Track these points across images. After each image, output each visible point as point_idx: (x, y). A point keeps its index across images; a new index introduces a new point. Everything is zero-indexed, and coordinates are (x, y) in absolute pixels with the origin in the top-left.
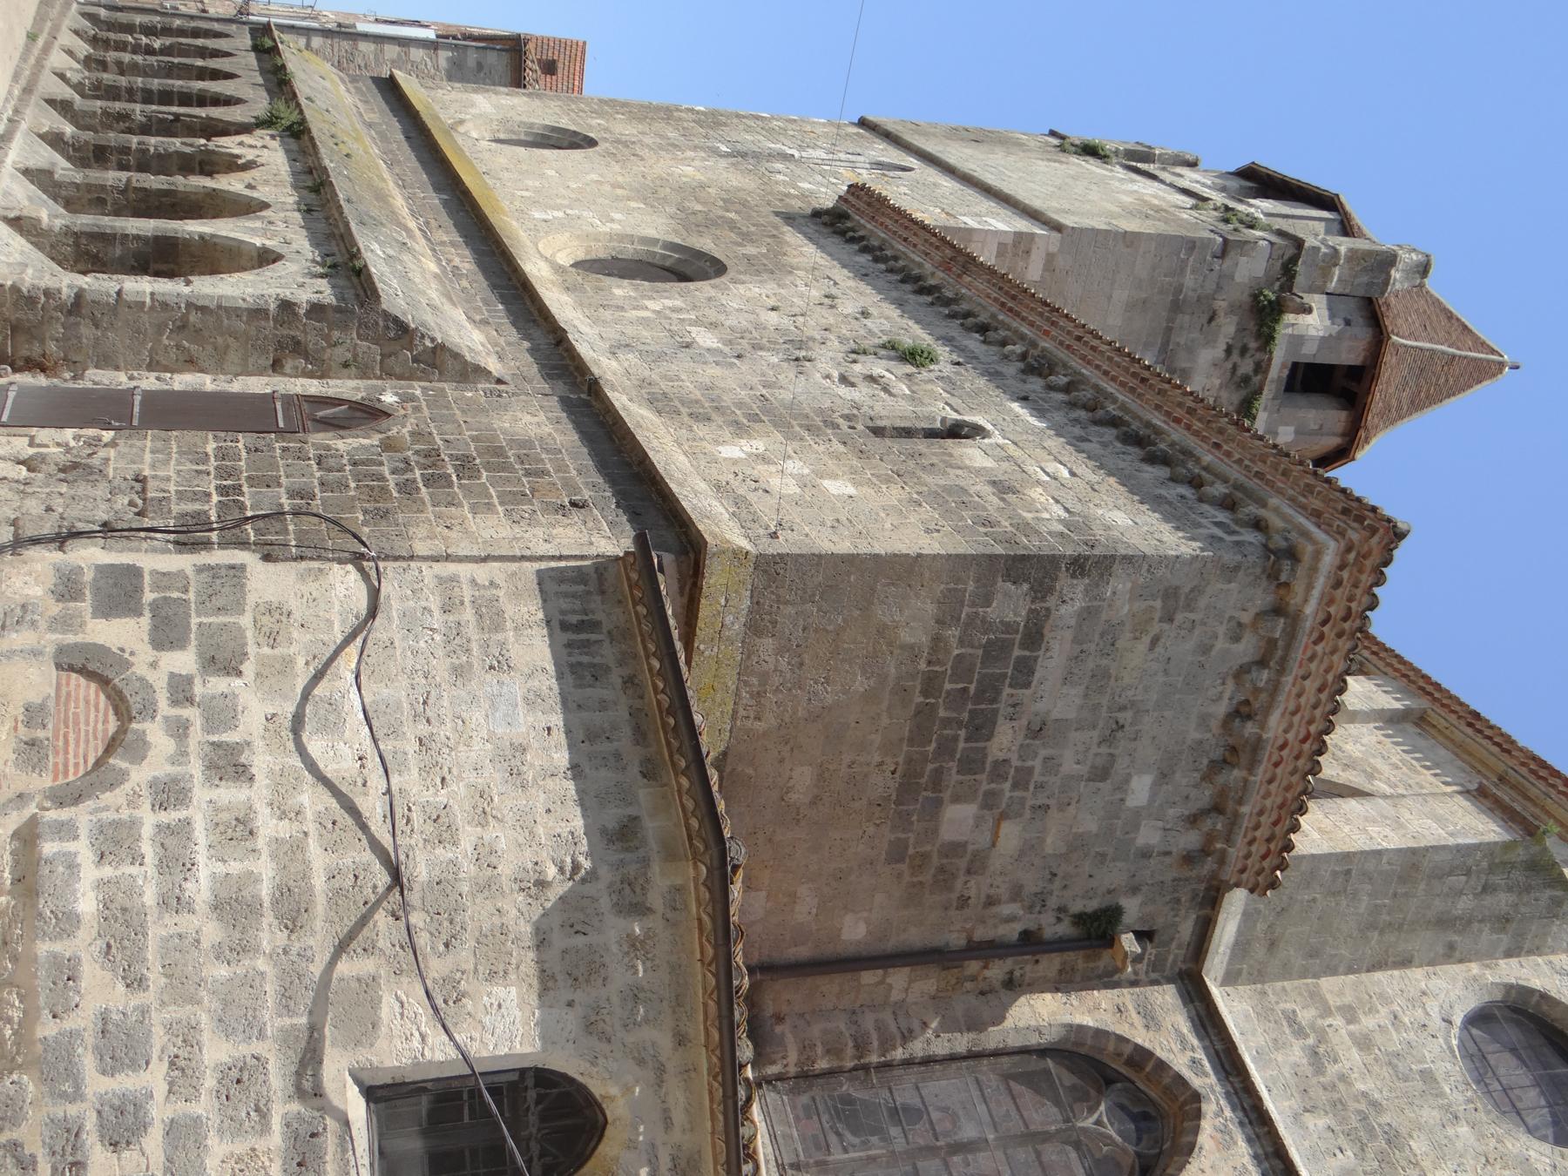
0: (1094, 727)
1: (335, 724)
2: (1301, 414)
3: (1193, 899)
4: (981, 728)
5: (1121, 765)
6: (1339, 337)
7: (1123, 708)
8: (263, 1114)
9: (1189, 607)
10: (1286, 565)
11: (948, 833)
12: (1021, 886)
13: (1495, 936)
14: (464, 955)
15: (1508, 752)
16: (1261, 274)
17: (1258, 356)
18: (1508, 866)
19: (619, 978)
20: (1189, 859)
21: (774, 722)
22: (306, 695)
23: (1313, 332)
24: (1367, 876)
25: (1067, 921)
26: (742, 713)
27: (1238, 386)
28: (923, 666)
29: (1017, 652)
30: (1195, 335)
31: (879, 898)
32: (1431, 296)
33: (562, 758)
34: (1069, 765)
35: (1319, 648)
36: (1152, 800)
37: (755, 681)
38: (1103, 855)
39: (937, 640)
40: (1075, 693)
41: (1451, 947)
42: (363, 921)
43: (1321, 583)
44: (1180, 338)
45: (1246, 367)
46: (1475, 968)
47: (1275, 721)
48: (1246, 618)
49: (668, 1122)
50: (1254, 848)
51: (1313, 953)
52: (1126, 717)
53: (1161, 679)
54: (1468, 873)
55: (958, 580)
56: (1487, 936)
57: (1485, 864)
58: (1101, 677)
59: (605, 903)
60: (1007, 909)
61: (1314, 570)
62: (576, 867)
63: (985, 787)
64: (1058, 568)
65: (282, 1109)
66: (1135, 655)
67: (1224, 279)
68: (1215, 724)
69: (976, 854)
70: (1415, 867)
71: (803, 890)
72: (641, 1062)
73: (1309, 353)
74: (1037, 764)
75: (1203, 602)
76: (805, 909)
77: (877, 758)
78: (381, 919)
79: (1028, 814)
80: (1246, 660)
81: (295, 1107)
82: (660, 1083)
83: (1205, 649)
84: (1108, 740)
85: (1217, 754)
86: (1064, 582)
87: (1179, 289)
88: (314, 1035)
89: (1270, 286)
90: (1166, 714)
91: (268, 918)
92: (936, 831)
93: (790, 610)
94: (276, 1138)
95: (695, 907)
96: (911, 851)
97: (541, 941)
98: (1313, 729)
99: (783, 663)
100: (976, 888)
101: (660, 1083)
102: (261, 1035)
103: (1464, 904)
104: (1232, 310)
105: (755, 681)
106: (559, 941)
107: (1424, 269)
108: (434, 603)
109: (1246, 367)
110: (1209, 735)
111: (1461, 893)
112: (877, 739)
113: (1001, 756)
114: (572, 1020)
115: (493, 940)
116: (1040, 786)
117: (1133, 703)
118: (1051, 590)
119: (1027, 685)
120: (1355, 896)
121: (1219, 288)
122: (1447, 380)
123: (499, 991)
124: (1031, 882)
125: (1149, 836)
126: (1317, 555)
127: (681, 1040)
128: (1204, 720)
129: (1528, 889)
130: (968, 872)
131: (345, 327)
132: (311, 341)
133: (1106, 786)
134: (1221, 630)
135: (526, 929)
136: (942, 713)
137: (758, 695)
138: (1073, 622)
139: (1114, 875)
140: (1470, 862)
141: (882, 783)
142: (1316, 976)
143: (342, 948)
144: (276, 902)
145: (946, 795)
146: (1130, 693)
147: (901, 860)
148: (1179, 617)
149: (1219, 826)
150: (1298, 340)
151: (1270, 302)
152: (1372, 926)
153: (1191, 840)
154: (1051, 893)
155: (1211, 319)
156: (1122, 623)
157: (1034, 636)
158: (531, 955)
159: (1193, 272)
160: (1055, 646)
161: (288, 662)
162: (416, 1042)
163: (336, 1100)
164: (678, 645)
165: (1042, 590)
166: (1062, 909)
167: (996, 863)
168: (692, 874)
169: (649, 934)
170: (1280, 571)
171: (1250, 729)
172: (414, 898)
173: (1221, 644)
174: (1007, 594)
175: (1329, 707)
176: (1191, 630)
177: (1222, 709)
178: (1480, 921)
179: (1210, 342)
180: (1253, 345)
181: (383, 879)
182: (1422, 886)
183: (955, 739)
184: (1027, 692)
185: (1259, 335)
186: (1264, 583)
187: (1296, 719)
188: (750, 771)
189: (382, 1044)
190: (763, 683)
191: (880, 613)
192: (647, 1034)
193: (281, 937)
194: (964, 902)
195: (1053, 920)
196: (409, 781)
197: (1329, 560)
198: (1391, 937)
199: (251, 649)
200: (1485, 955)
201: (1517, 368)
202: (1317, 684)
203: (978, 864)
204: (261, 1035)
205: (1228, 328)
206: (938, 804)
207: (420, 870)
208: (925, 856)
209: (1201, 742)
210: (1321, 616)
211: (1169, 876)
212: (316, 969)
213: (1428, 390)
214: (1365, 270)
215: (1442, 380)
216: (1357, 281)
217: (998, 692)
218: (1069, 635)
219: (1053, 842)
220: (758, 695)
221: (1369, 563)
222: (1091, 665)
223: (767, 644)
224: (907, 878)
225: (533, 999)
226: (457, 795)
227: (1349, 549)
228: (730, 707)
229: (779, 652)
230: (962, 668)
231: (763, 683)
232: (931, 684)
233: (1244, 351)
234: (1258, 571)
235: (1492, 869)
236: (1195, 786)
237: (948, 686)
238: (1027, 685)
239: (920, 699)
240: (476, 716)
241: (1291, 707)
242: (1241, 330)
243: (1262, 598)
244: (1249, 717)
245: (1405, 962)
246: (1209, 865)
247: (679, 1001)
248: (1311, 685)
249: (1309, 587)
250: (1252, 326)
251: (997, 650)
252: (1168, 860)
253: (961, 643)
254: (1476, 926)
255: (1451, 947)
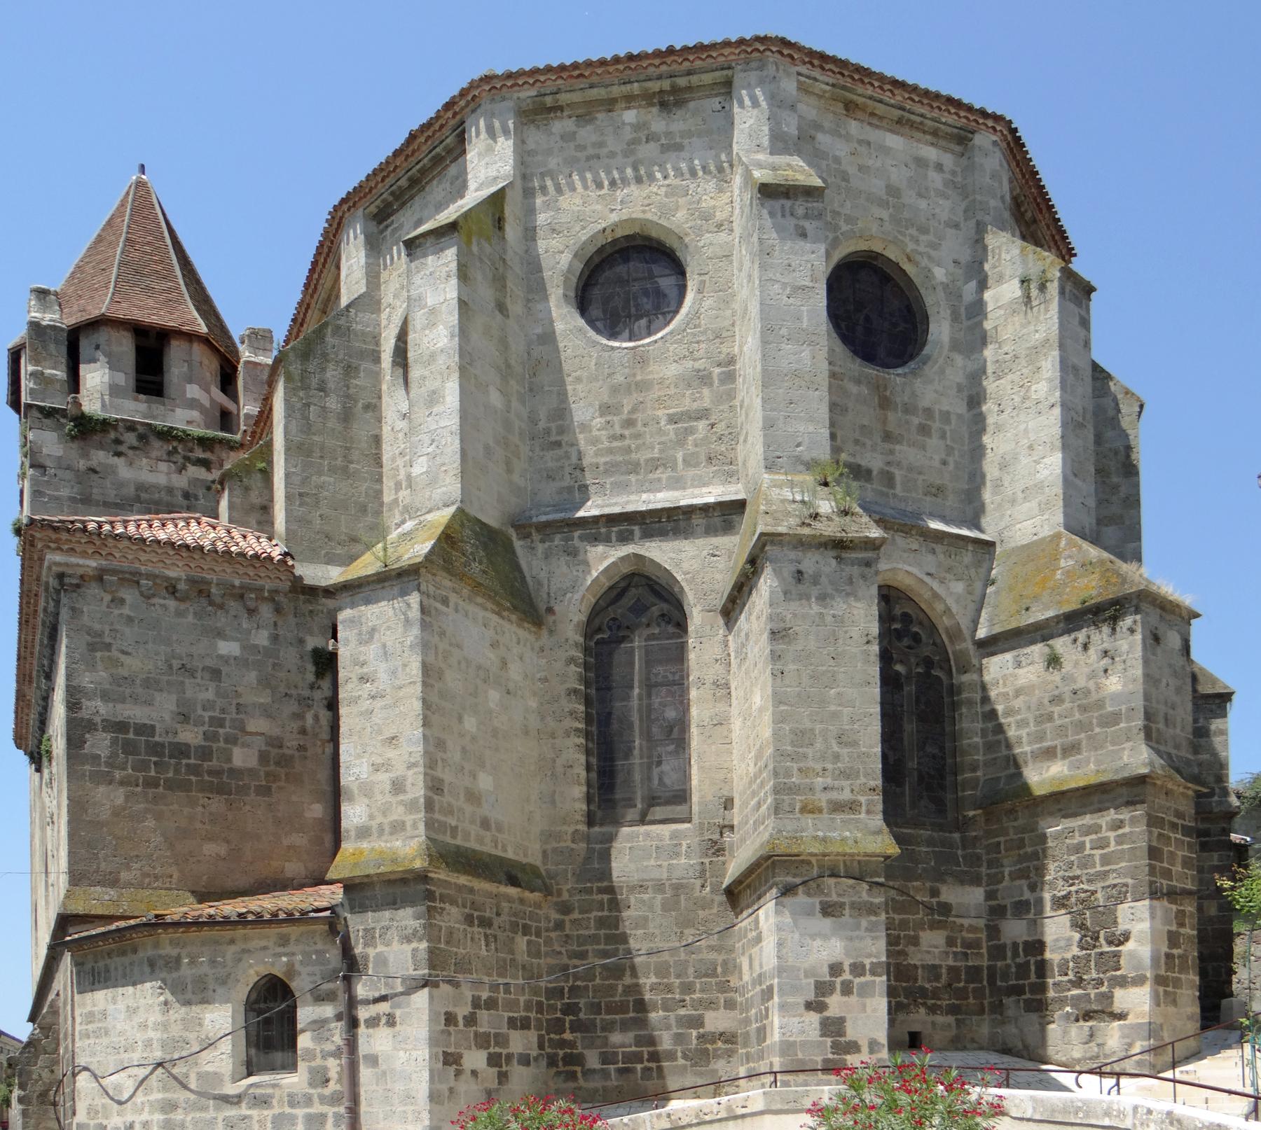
0: (183, 682)
1: (118, 1088)
2: (175, 379)
3: (310, 602)
4: (181, 751)
5: (209, 662)
6: (109, 355)
7: (170, 667)
8: (244, 1118)
9: (100, 635)
10: (67, 580)
11: (253, 762)
12: (294, 714)
13: (362, 374)
14: (191, 1036)
15: (308, 305)
16: (55, 434)
17: (121, 430)
18: (305, 374)
19: (206, 969)
20: (278, 610)
21: (174, 868)
22: (112, 1099)
23: (106, 379)
24: (305, 480)
25: (321, 682)
26: (168, 885)
27: (147, 443)
28: (139, 789)
29: (131, 736)
30: (108, 483)
31: (294, 798)
32: (85, 257)
33: (130, 989)
34: (210, 695)
35: (117, 555)
36: (237, 640)
37: (147, 880)
38: (274, 665)
39: (122, 783)
40: (159, 697)
41: (367, 407)
42: (175, 1078)
43: (74, 560)
44: (111, 495)
45: (130, 438)
46: (384, 387)
47: (172, 573)
48: (108, 598)
49: (265, 948)
50: (263, 575)
51: (363, 509)
52: (176, 664)
53: (150, 646)
54: (308, 405)
55: (84, 775)
56: (360, 381)
57: (301, 394)
58: (148, 683)
59: (175, 975)
60: (309, 720)
61: (67, 565)
62: (160, 988)
63: (222, 744)
64: (75, 718)
65: (244, 1110)
66: (133, 664)
67: (59, 461)
68: (183, 606)
69: (268, 744)
70: (300, 447)
71: (286, 842)
72: (240, 960)
73: (125, 378)
74: (207, 715)
75: (97, 627)
76: (299, 840)
77: (200, 809)
78: (175, 1071)
79: (241, 716)
80: (137, 593)
81: (244, 1105)
82: (249, 951)
83: (130, 620)
84: (192, 673)
85: (204, 602)
86: (84, 714)
87: (73, 500)
88: (215, 1098)
89: (63, 426)
90: (175, 638)
91: (172, 1116)
92: (250, 770)
93: (103, 866)
94: (254, 1113)
95: (178, 934)
96: (264, 783)
97: (188, 1003)
98: (172, 553)
99: (135, 866)
100: (292, 742)
101: (249, 951)
102: (215, 1118)
103: (333, 403)
104: (86, 455)
105: (147, 880)
106: (189, 996)
107: (42, 294)
108: (88, 1042)
109: (130, 438)
110: (191, 610)
111: (324, 408)
112: (186, 810)
113: (201, 736)
114: (220, 991)
115: (187, 1024)
116: (223, 711)
117: (167, 661)
118: (90, 721)
119: (153, 727)
120: (320, 487)
121: (68, 468)
122: (149, 243)
123: (207, 1022)
124: (292, 707)
125: (262, 638)
126: (59, 564)
127: (232, 941)
128: (179, 614)
129: (325, 355)
130: (281, 747)
131: (30, 1073)
132: (39, 1088)
133: (225, 669)
134: (116, 612)
135: (183, 1010)
136: (170, 775)
137: (156, 878)
138: (111, 705)
139: (290, 656)
140: (299, 405)
141: (217, 804)
142: (382, 504)
143: (185, 1087)
144: (166, 1113)
145: (226, 766)
146: (160, 663)
147: (269, 788)
148: (108, 640)
149: (253, 596)
150: (114, 390)
151: (75, 426)
152: (345, 470)
153: (266, 611)
154: (299, 695)
155: (94, 471)
156: (112, 675)
157: (120, 727)
158: (193, 1007)
159: (57, 490)
160: (127, 713)
161: (104, 1106)
162: (224, 1056)
163: (242, 1089)
164: (113, 927)
165: (90, 726)
166: (312, 687)
167: (276, 731)
168: (164, 936)
169: (188, 956)
170: (71, 584)
171: (182, 586)
172: (168, 1057)
173: (126, 611)
174: (92, 746)
175: (155, 545)
176: (116, 631)
177: (172, 604)
178: (348, 388)
179: (113, 470)
180: (113, 435)
181: (160, 1070)
182: (316, 438)
183: (188, 765)
184: (158, 726)
185: (105, 431)
186: (83, 589)
187: (168, 562)
188: (205, 878)
189: (223, 1071)
190: (148, 875)
191: (105, 815)
192: (229, 956)
193: (180, 1111)
194: (301, 748)
195: (319, 692)
196: (136, 1057)
197: (58, 558)
198: (355, 455)
199: (100, 1121)
200: (377, 377)
201: (143, 166)
202: (142, 553)
203: (276, 743)
204: (215, 1118)
205: (100, 457)
206: (234, 772)
207: (158, 1055)
208: (267, 774)
209: (195, 614)
210: (97, 556)
211: (292, 620)
212: (193, 1097)
213: (156, 262)
214: (45, 348)
215: (147, 249)
216: (54, 353)
217: (157, 744)
218: (119, 706)
219: (264, 698)
220: (156, 878)
221: (54, 536)
222: (140, 690)
223: (124, 876)
224: (282, 784)
225: (211, 1007)
226: (140, 1036)
227: (49, 547)
228: (163, 892)
229: (129, 868)
230: (142, 766)
231: (148, 875)
232: (151, 783)
233: (118, 442)
234: (75, 595)
235: (306, 388)
236: (227, 612)
237: (153, 773)
238: (153, 727)
239: (161, 789)
240: (119, 1027)
241: (161, 565)
242: (101, 447)
243: (93, 590)
244: (174, 587)
245: (377, 440)
246: (280, 598)
247: (217, 942)
248: (143, 557)
249: (78, 565)
250: (97, 438)
251: (130, 748)
252: (280, 623)
253: (124, 769)
254: (352, 391)
255: (367, 407)
